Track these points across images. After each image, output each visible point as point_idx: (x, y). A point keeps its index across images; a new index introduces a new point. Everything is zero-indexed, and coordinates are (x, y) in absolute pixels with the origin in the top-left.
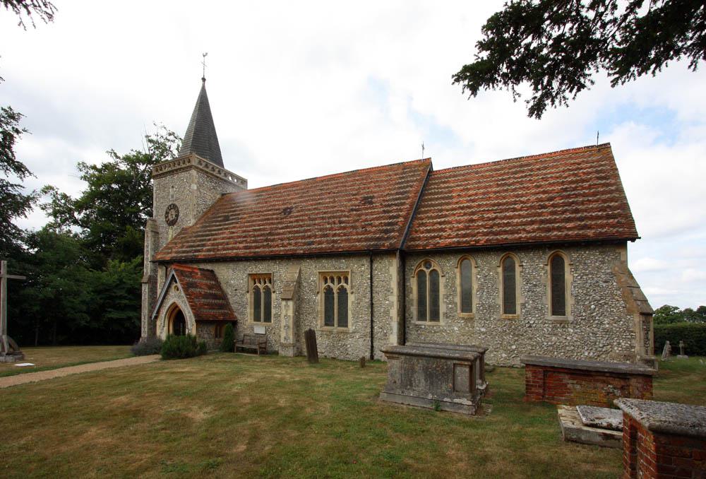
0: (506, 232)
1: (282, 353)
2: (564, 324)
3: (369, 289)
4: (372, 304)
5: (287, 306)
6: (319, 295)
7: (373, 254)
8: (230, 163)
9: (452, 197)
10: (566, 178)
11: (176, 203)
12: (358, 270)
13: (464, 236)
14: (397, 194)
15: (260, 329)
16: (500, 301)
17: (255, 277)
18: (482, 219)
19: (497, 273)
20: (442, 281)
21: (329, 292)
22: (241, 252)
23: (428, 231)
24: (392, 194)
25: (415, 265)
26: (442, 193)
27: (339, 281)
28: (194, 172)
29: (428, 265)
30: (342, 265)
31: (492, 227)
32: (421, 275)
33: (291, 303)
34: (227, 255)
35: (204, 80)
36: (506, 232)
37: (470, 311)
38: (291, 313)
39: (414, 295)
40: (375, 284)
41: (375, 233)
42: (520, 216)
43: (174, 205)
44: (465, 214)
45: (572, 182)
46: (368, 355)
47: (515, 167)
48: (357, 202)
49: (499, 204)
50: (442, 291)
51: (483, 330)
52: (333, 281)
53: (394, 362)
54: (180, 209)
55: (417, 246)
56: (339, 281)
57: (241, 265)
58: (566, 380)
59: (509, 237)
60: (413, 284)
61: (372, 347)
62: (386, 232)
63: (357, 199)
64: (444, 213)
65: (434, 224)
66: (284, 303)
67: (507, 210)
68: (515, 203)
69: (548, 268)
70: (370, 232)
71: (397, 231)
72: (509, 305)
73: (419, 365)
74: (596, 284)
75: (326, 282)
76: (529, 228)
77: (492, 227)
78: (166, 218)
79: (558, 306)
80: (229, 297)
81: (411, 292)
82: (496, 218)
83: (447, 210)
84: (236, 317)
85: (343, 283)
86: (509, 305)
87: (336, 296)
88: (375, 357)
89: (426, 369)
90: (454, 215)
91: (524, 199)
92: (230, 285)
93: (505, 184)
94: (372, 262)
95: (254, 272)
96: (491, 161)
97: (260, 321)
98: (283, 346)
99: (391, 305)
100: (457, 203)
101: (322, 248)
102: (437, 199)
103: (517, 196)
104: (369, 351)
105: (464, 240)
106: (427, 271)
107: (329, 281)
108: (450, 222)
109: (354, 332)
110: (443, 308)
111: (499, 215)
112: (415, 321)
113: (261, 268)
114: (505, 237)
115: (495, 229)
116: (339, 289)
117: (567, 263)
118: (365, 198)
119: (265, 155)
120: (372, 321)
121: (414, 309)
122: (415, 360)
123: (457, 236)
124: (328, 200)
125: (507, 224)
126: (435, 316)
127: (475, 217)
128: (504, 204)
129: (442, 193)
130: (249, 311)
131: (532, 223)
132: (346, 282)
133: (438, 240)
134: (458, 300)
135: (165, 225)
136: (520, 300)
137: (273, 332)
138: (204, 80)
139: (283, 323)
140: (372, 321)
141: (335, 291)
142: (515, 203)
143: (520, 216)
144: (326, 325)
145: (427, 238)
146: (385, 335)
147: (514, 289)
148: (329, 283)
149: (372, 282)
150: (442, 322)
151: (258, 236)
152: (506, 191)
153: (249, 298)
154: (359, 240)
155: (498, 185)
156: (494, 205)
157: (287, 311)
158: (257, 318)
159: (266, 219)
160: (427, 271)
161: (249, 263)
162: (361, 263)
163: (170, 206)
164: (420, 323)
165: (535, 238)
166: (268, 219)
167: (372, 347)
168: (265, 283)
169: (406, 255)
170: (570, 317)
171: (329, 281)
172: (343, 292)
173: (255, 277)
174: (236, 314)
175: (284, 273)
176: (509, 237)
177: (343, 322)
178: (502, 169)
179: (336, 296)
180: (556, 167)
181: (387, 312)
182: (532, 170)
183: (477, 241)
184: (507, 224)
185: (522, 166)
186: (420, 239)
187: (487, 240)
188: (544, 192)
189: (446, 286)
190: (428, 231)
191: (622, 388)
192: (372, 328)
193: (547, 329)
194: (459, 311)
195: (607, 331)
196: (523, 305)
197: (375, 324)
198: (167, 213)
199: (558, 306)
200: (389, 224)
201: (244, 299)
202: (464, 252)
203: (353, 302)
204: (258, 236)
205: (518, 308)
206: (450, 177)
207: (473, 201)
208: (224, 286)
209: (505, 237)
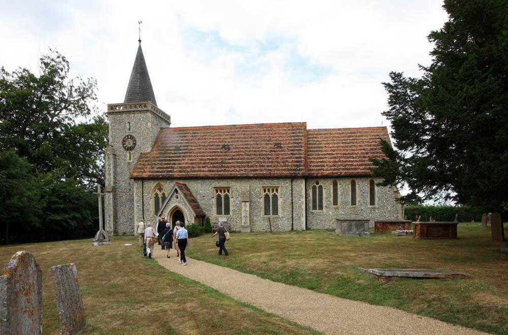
0: (352, 169)
1: (243, 230)
2: (374, 209)
3: (291, 195)
4: (292, 203)
5: (246, 205)
6: (262, 199)
7: (293, 178)
8: (163, 103)
9: (322, 147)
10: (371, 143)
11: (133, 135)
12: (284, 188)
13: (335, 170)
14: (294, 143)
15: (222, 219)
16: (350, 200)
17: (217, 189)
18: (340, 161)
19: (349, 187)
20: (324, 191)
21: (267, 197)
22: (208, 174)
23: (316, 166)
24: (291, 143)
25: (312, 183)
26: (316, 144)
27: (273, 191)
28: (149, 114)
29: (317, 183)
30: (275, 183)
31: (345, 166)
32: (314, 188)
33: (248, 204)
34: (198, 176)
35: (140, 41)
36: (352, 169)
37: (337, 205)
38: (248, 209)
39: (311, 198)
40: (294, 192)
41: (291, 166)
42: (356, 161)
43: (131, 136)
44: (331, 158)
45: (374, 145)
46: (290, 228)
47: (348, 133)
48: (272, 146)
49: (346, 154)
50: (324, 195)
51: (343, 213)
52: (221, 192)
53: (345, 223)
54: (137, 139)
55: (313, 174)
56: (273, 191)
57: (207, 182)
58: (389, 225)
59: (354, 171)
60: (310, 192)
61: (292, 224)
62: (297, 166)
63: (271, 144)
64: (321, 156)
65: (318, 162)
66: (243, 204)
67: (350, 157)
68: (352, 154)
69: (369, 185)
70: (288, 166)
71: (303, 166)
72: (354, 202)
73: (353, 223)
74: (386, 192)
75: (217, 192)
76: (361, 167)
77: (345, 166)
78: (123, 144)
79: (372, 202)
80: (198, 201)
81: (309, 196)
82: (346, 161)
83: (322, 155)
84: (205, 213)
85: (275, 192)
86: (354, 202)
87: (271, 199)
88: (294, 229)
89: (355, 225)
90: (326, 158)
91: (356, 152)
92: (199, 194)
93: (346, 143)
94: (292, 181)
95: (217, 186)
96: (337, 128)
97: (222, 214)
98: (244, 227)
99: (302, 203)
100: (326, 151)
101: (264, 174)
102: (315, 147)
103: (353, 150)
104: (291, 226)
105: (335, 172)
106: (317, 186)
107: (267, 191)
108: (325, 162)
109: (282, 217)
110: (325, 204)
111: (347, 160)
112: (311, 210)
113: (223, 184)
114: (352, 171)
115: (347, 167)
116: (217, 196)
117: (338, 183)
118: (276, 144)
119: (192, 101)
120: (292, 211)
121: (311, 205)
122: (352, 222)
123: (331, 170)
124: (252, 143)
125: (352, 165)
126: (321, 208)
127: (337, 160)
128: (348, 154)
129: (316, 144)
130: (214, 209)
131: (362, 165)
132: (228, 192)
133: (322, 171)
134: (332, 199)
135: (122, 149)
136: (358, 200)
137: (232, 220)
138: (140, 41)
139: (243, 215)
140: (292, 211)
141: (223, 197)
142: (352, 154)
143: (356, 161)
144: (265, 214)
145: (317, 170)
146: (299, 218)
147: (333, 197)
148: (219, 193)
149: (292, 192)
150: (324, 210)
151: (215, 163)
152: (347, 147)
153: (214, 201)
154: (284, 170)
155: (343, 143)
156: (344, 154)
157: (245, 208)
158: (219, 212)
159: (213, 152)
160: (317, 186)
161: (213, 181)
162: (286, 182)
163: (128, 136)
164: (313, 211)
165: (364, 172)
166: (215, 152)
167: (292, 224)
168: (225, 192)
169: (307, 178)
170: (376, 206)
171: (267, 191)
172: (275, 197)
173: (217, 189)
174: (204, 211)
175: (238, 188)
176: (354, 171)
177: (276, 212)
178: (342, 133)
179: (271, 199)
180: (367, 136)
181: (300, 207)
182: (356, 136)
183: (341, 173)
184: (352, 165)
185: (351, 133)
186: (313, 170)
187: (345, 173)
188: (364, 149)
189: (326, 193)
190: (316, 166)
191: (403, 227)
192: (292, 214)
193: (368, 211)
194: (332, 205)
195: (389, 211)
196: (359, 201)
197: (294, 213)
198: (124, 141)
199: (372, 202)
200: (297, 162)
201: (211, 202)
202: (335, 178)
203: (281, 202)
204: (215, 163)
205: (357, 203)
206: (317, 134)
207: (333, 151)
208: (194, 194)
209: (352, 171)
